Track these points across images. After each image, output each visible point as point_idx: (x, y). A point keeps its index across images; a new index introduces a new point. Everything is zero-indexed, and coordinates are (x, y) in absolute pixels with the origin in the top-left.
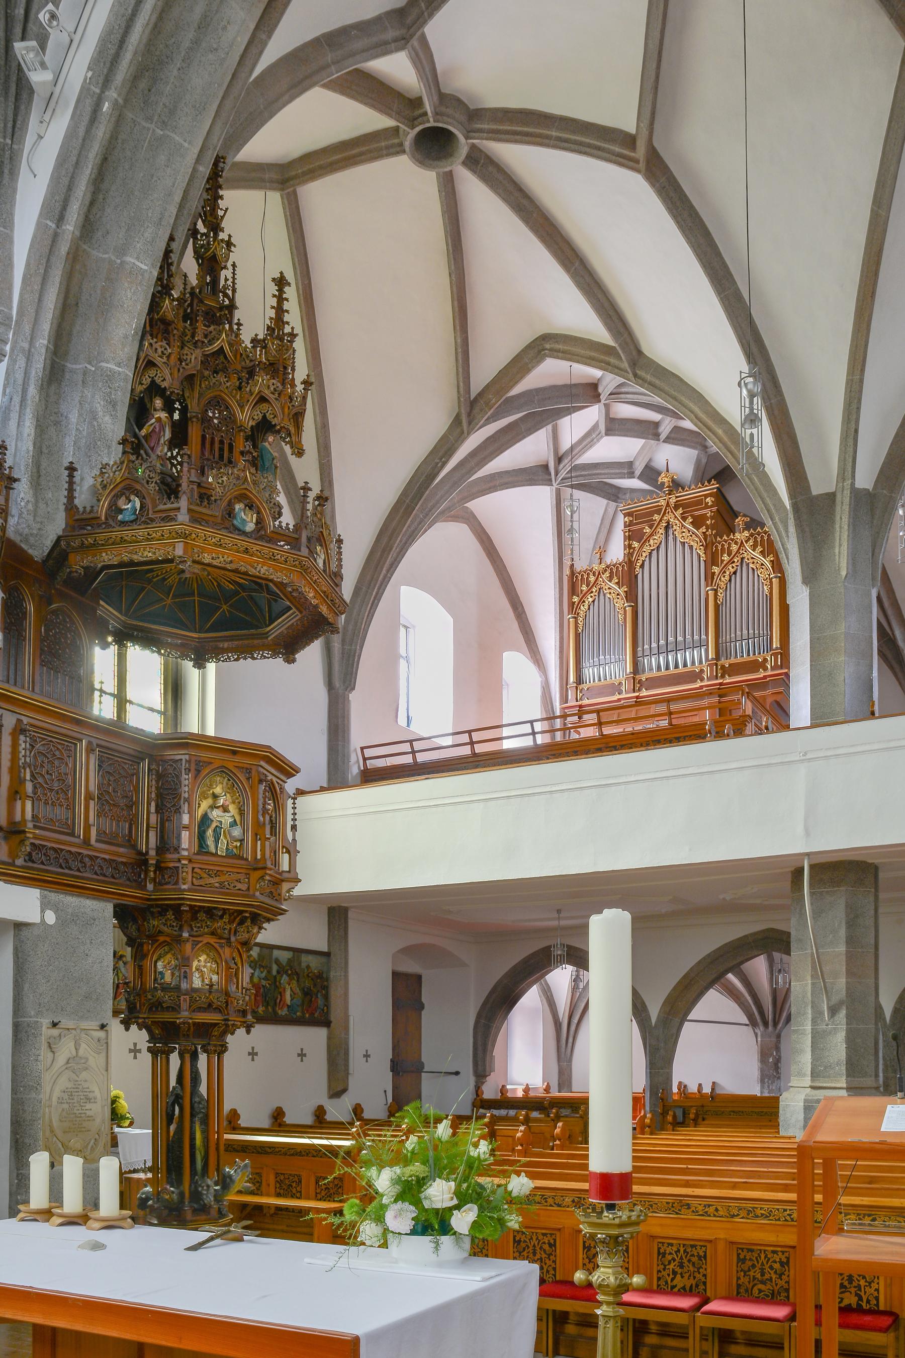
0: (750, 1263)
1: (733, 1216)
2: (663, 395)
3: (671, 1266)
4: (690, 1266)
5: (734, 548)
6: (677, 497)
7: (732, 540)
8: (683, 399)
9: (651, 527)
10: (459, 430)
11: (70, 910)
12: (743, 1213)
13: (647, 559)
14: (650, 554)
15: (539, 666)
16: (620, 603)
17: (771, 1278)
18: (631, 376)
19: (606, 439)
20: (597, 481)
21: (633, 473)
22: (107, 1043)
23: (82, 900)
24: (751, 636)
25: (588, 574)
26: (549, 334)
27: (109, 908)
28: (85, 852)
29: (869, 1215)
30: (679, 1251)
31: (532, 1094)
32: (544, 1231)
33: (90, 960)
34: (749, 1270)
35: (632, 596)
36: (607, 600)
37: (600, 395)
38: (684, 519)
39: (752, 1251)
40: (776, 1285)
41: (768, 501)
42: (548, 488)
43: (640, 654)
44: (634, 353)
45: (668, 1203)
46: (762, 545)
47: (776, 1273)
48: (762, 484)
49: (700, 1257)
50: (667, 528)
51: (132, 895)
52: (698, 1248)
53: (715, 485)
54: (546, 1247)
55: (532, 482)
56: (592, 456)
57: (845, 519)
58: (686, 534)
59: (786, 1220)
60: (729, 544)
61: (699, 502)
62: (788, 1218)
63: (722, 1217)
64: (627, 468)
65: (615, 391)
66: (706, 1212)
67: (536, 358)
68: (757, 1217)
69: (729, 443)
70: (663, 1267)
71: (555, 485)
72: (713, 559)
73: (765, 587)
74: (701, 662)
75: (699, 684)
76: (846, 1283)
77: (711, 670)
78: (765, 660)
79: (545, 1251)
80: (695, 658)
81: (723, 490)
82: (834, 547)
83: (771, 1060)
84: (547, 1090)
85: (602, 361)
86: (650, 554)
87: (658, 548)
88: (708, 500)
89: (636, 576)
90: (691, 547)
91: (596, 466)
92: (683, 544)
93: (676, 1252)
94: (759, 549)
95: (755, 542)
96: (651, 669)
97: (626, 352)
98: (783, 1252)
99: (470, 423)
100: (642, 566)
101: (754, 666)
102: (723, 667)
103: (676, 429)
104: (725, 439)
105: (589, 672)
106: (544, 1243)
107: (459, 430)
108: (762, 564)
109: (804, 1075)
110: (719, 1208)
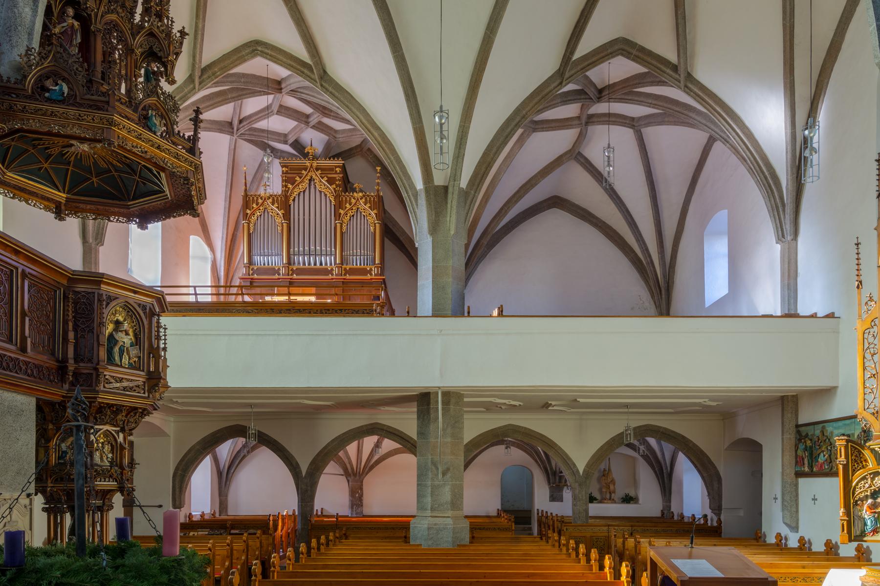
5: (353, 201)
10: (192, 86)
11: (6, 404)
14: (299, 194)
16: (279, 220)
18: (319, 84)
19: (276, 116)
20: (262, 141)
22: (31, 509)
23: (14, 394)
27: (33, 401)
28: (22, 358)
31: (206, 517)
33: (20, 443)
35: (287, 216)
37: (281, 89)
42: (228, 137)
43: (292, 252)
46: (370, 203)
50: (310, 180)
51: (55, 393)
55: (221, 131)
56: (262, 124)
57: (455, 203)
58: (323, 187)
61: (332, 170)
64: (283, 138)
71: (235, 136)
72: (339, 205)
74: (331, 264)
75: (330, 276)
80: (328, 261)
86: (299, 194)
87: (304, 191)
90: (326, 195)
91: (263, 131)
92: (321, 192)
94: (368, 205)
95: (366, 199)
96: (299, 263)
97: (314, 69)
99: (200, 83)
100: (294, 200)
101: (364, 272)
102: (345, 269)
103: (320, 123)
104: (380, 139)
105: (257, 259)
107: (192, 86)
109: (426, 509)
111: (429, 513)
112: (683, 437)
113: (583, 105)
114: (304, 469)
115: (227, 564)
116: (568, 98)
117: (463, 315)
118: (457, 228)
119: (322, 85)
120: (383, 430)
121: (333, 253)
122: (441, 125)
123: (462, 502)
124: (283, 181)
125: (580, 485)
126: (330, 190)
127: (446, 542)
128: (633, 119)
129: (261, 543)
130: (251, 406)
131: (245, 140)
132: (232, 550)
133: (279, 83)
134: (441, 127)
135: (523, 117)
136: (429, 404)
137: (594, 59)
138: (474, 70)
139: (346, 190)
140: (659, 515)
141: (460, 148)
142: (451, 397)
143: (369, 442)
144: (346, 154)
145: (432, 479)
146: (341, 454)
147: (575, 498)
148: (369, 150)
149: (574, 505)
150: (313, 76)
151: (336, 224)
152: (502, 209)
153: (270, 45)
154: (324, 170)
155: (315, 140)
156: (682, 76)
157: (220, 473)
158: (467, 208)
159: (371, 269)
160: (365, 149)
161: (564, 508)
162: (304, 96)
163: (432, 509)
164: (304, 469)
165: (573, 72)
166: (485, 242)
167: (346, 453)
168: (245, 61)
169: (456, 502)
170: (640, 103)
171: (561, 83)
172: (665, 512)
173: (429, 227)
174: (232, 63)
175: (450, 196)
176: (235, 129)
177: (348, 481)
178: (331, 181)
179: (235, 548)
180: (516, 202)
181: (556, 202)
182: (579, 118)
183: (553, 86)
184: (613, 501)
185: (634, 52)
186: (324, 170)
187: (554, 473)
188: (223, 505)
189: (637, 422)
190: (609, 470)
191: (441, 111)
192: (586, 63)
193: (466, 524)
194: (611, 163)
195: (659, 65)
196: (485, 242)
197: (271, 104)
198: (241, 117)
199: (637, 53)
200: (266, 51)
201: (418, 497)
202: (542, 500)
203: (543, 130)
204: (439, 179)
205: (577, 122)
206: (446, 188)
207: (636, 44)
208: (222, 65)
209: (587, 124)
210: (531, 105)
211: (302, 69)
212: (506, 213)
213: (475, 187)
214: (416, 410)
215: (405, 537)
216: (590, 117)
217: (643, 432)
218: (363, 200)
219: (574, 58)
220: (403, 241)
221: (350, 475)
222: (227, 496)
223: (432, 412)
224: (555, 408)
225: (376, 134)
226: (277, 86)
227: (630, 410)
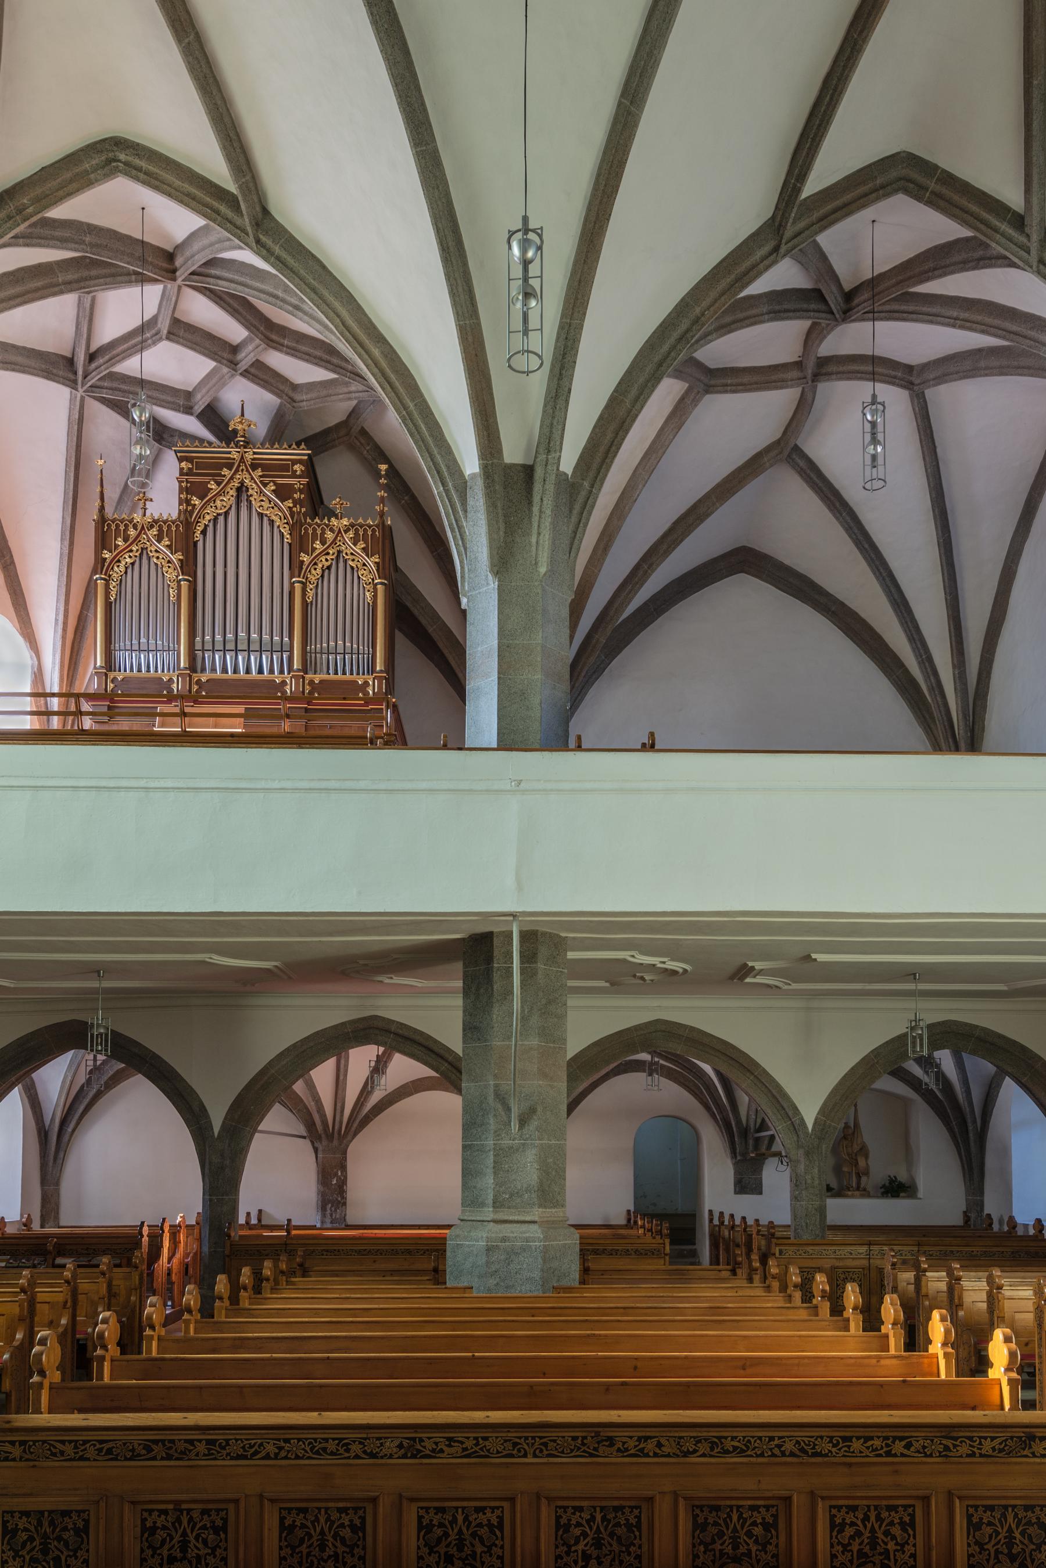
0: (714, 1530)
1: (687, 1454)
2: (297, 280)
3: (580, 1547)
4: (614, 1543)
5: (329, 536)
6: (255, 453)
7: (327, 526)
8: (326, 293)
9: (218, 484)
12: (703, 1448)
13: (211, 525)
14: (215, 520)
15: (30, 643)
16: (171, 574)
17: (750, 1551)
18: (251, 240)
21: (191, 408)
24: (348, 650)
25: (126, 526)
26: (126, 140)
29: (901, 1439)
30: (593, 1518)
32: (341, 1505)
34: (714, 1542)
35: (189, 566)
36: (153, 567)
37: (174, 271)
38: (265, 485)
39: (717, 1508)
40: (758, 1561)
41: (439, 458)
42: (65, 392)
43: (198, 646)
44: (258, 209)
45: (574, 1438)
46: (365, 541)
47: (756, 1542)
48: (431, 435)
49: (629, 1526)
50: (239, 490)
52: (627, 1511)
53: (304, 452)
54: (346, 1533)
58: (266, 504)
59: (773, 1455)
60: (323, 530)
62: (776, 1451)
63: (668, 1456)
64: (181, 399)
65: (202, 270)
66: (642, 1450)
67: (103, 167)
68: (727, 1452)
69: (388, 371)
70: (565, 1549)
72: (300, 543)
73: (367, 594)
76: (867, 1549)
77: (297, 684)
78: (366, 683)
79: (343, 1541)
81: (314, 459)
82: (529, 534)
83: (334, 1182)
84: (27, 1224)
85: (206, 205)
86: (215, 520)
87: (226, 514)
88: (297, 467)
89: (195, 544)
92: (261, 516)
93: (588, 1521)
95: (356, 533)
97: (242, 204)
98: (767, 1508)
100: (204, 532)
102: (311, 682)
103: (259, 364)
106: (342, 1526)
108: (364, 565)
109: (483, 1205)
110: (663, 1441)
111: (488, 1213)
112: (1024, 1049)
113: (814, 325)
114: (217, 1120)
115: (19, 1336)
116: (781, 305)
117: (565, 748)
118: (552, 561)
119: (258, 241)
120: (388, 1031)
121: (286, 648)
122: (526, 263)
123: (563, 1187)
124: (181, 492)
125: (807, 1154)
126: (279, 512)
127: (527, 1281)
128: (909, 369)
129: (110, 1285)
130: (97, 970)
131: (103, 401)
132: (32, 1303)
133: (170, 257)
134: (526, 269)
135: (696, 321)
136: (489, 960)
137: (848, 197)
138: (593, 195)
139: (315, 514)
140: (959, 1221)
141: (560, 378)
142: (541, 940)
143: (361, 1058)
144: (320, 442)
145: (497, 1134)
146: (299, 1087)
147: (796, 1183)
148: (363, 432)
149: (795, 1198)
150: (238, 221)
151: (292, 585)
152: (637, 567)
153: (145, 148)
154: (269, 469)
155: (247, 402)
156: (1035, 237)
157: (43, 1134)
158: (574, 519)
159: (366, 683)
160: (355, 430)
161: (775, 1201)
162: (222, 286)
163: (497, 1204)
164: (217, 1120)
165: (801, 225)
166: (602, 639)
167: (311, 1086)
168: (90, 184)
169: (549, 1191)
170: (932, 318)
171: (776, 249)
172: (973, 1215)
173: (491, 557)
174: (61, 187)
175: (537, 487)
176: (80, 372)
177: (316, 1150)
178: (283, 492)
179: (40, 1297)
180: (667, 553)
181: (744, 560)
182: (799, 365)
183: (760, 254)
184: (865, 1194)
185: (932, 185)
186: (269, 469)
187: (745, 1132)
188: (50, 1205)
189: (936, 1012)
190: (856, 1125)
191: (526, 230)
192: (830, 207)
193: (573, 1240)
194: (880, 436)
195: (985, 215)
196: (602, 639)
197: (154, 319)
198: (93, 348)
199: (938, 188)
200: (137, 162)
201: (464, 1175)
202: (718, 1193)
203: (725, 389)
204: (513, 453)
205: (795, 374)
206: (528, 471)
207: (936, 167)
208: (39, 191)
209: (816, 377)
210: (713, 294)
211: (216, 204)
212: (646, 576)
213: (591, 474)
214: (459, 984)
215: (436, 1270)
216: (824, 362)
217: (946, 1034)
218: (351, 534)
219: (805, 194)
220: (435, 636)
221: (320, 1138)
222: (57, 1183)
223: (496, 976)
224: (759, 980)
225: (376, 352)
226: (162, 262)
227: (922, 986)
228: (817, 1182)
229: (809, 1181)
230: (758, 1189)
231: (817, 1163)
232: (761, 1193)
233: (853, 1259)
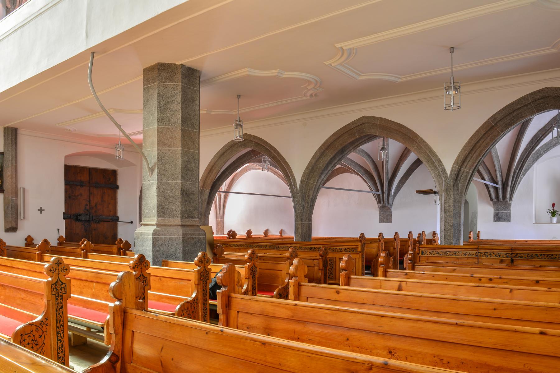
228: (452, 208)
229: (447, 208)
230: (507, 219)
231: (452, 196)
232: (509, 221)
233: (467, 258)
